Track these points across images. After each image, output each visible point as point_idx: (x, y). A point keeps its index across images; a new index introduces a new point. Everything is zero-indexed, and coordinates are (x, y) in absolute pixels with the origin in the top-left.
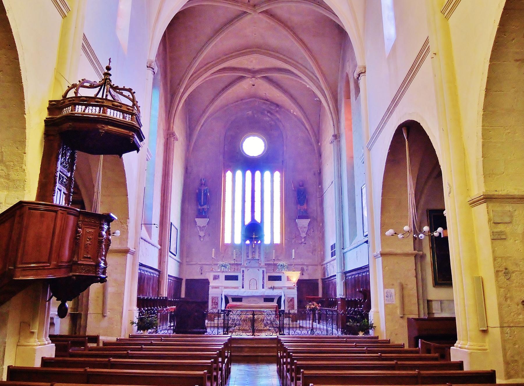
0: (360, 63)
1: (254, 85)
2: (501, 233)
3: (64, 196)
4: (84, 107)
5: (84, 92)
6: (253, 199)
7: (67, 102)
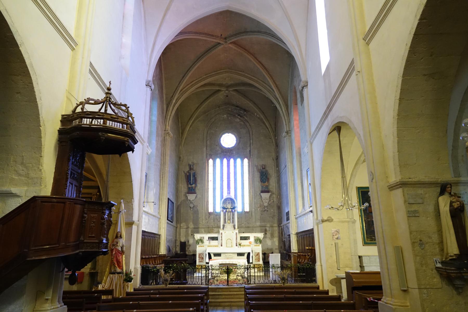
0: (303, 78)
1: (227, 96)
2: (416, 211)
3: (75, 188)
4: (91, 120)
5: (89, 108)
6: (229, 180)
7: (75, 116)
